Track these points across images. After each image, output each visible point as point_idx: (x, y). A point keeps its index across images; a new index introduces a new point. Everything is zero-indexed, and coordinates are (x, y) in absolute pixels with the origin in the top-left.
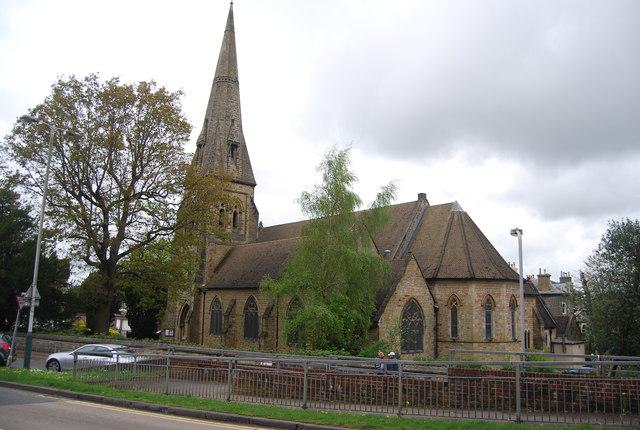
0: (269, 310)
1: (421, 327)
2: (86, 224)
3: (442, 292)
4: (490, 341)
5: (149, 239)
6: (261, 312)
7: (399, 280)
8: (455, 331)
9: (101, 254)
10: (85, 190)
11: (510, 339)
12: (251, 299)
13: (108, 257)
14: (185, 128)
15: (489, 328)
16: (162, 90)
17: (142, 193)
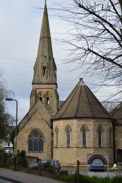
4: (68, 147)
11: (81, 146)
15: (68, 141)
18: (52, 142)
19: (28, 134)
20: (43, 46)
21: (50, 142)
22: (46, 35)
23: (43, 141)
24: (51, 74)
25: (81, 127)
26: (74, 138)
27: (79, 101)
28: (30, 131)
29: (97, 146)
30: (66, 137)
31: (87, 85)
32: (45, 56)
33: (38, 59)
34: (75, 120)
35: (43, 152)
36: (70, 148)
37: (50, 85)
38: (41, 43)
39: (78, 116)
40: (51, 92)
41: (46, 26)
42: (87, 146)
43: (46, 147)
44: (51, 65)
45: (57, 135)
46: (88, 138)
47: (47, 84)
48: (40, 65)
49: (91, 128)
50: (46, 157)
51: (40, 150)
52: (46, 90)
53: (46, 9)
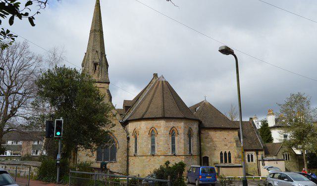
4: (153, 155)
11: (170, 154)
15: (153, 148)
18: (128, 149)
20: (95, 40)
21: (125, 148)
22: (98, 29)
23: (116, 148)
24: (103, 72)
25: (170, 129)
26: (161, 143)
27: (163, 98)
29: (188, 153)
30: (150, 142)
31: (167, 80)
33: (87, 54)
34: (163, 121)
35: (116, 161)
36: (155, 157)
37: (102, 84)
38: (93, 36)
39: (167, 116)
41: (99, 18)
42: (177, 152)
43: (120, 155)
44: (104, 61)
45: (136, 139)
46: (178, 143)
49: (181, 131)
50: (120, 168)
51: (112, 159)
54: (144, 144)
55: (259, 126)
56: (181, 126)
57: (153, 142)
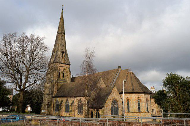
0: (72, 103)
1: (117, 108)
2: (15, 78)
3: (124, 96)
4: (140, 112)
5: (69, 84)
6: (70, 104)
7: (110, 93)
8: (129, 109)
9: (20, 87)
10: (15, 68)
11: (147, 111)
12: (67, 100)
13: (22, 88)
14: (46, 48)
15: (139, 108)
16: (38, 37)
17: (32, 68)
19: (111, 102)
28: (112, 101)
32: (63, 45)
40: (67, 69)
42: (141, 110)
47: (65, 64)
48: (60, 50)
52: (64, 68)
53: (62, 17)
54: (134, 106)
55: (58, 69)
56: (143, 97)
57: (139, 105)
